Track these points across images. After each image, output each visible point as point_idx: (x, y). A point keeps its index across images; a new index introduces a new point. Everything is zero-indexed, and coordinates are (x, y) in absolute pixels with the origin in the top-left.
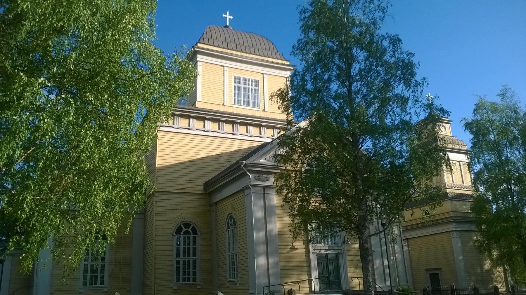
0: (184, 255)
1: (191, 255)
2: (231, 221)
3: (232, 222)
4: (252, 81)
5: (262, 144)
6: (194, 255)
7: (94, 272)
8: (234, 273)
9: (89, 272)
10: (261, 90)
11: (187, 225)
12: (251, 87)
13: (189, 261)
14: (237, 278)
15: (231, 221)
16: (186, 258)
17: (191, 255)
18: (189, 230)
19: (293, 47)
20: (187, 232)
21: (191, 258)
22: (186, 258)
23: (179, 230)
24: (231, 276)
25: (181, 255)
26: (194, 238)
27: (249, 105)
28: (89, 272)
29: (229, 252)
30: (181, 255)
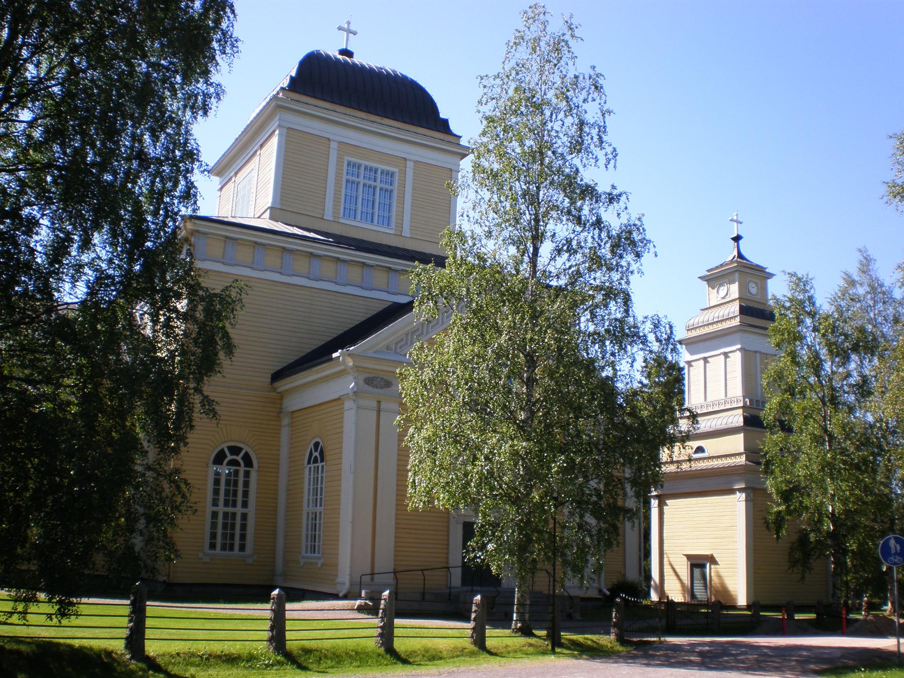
0: (226, 504)
1: (239, 503)
2: (316, 450)
3: (317, 454)
4: (382, 172)
5: (389, 306)
6: (245, 504)
7: (229, 526)
8: (313, 544)
9: (220, 526)
10: (395, 194)
11: (235, 450)
12: (379, 185)
13: (234, 514)
14: (319, 553)
15: (316, 450)
16: (230, 509)
17: (239, 503)
18: (239, 458)
19: (508, 44)
20: (233, 463)
21: (239, 510)
22: (230, 509)
23: (219, 459)
24: (309, 550)
25: (239, 517)
26: (247, 474)
27: (372, 222)
28: (220, 526)
29: (308, 506)
30: (239, 517)
